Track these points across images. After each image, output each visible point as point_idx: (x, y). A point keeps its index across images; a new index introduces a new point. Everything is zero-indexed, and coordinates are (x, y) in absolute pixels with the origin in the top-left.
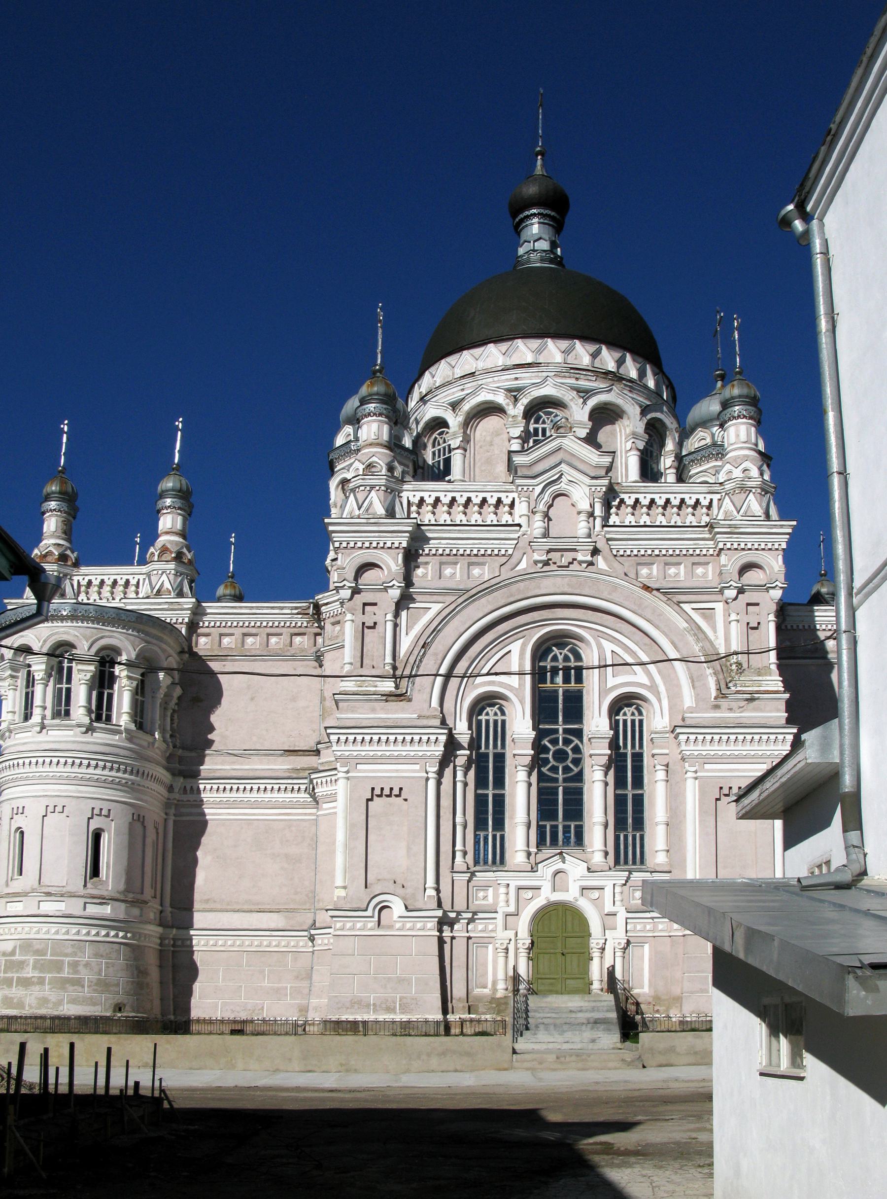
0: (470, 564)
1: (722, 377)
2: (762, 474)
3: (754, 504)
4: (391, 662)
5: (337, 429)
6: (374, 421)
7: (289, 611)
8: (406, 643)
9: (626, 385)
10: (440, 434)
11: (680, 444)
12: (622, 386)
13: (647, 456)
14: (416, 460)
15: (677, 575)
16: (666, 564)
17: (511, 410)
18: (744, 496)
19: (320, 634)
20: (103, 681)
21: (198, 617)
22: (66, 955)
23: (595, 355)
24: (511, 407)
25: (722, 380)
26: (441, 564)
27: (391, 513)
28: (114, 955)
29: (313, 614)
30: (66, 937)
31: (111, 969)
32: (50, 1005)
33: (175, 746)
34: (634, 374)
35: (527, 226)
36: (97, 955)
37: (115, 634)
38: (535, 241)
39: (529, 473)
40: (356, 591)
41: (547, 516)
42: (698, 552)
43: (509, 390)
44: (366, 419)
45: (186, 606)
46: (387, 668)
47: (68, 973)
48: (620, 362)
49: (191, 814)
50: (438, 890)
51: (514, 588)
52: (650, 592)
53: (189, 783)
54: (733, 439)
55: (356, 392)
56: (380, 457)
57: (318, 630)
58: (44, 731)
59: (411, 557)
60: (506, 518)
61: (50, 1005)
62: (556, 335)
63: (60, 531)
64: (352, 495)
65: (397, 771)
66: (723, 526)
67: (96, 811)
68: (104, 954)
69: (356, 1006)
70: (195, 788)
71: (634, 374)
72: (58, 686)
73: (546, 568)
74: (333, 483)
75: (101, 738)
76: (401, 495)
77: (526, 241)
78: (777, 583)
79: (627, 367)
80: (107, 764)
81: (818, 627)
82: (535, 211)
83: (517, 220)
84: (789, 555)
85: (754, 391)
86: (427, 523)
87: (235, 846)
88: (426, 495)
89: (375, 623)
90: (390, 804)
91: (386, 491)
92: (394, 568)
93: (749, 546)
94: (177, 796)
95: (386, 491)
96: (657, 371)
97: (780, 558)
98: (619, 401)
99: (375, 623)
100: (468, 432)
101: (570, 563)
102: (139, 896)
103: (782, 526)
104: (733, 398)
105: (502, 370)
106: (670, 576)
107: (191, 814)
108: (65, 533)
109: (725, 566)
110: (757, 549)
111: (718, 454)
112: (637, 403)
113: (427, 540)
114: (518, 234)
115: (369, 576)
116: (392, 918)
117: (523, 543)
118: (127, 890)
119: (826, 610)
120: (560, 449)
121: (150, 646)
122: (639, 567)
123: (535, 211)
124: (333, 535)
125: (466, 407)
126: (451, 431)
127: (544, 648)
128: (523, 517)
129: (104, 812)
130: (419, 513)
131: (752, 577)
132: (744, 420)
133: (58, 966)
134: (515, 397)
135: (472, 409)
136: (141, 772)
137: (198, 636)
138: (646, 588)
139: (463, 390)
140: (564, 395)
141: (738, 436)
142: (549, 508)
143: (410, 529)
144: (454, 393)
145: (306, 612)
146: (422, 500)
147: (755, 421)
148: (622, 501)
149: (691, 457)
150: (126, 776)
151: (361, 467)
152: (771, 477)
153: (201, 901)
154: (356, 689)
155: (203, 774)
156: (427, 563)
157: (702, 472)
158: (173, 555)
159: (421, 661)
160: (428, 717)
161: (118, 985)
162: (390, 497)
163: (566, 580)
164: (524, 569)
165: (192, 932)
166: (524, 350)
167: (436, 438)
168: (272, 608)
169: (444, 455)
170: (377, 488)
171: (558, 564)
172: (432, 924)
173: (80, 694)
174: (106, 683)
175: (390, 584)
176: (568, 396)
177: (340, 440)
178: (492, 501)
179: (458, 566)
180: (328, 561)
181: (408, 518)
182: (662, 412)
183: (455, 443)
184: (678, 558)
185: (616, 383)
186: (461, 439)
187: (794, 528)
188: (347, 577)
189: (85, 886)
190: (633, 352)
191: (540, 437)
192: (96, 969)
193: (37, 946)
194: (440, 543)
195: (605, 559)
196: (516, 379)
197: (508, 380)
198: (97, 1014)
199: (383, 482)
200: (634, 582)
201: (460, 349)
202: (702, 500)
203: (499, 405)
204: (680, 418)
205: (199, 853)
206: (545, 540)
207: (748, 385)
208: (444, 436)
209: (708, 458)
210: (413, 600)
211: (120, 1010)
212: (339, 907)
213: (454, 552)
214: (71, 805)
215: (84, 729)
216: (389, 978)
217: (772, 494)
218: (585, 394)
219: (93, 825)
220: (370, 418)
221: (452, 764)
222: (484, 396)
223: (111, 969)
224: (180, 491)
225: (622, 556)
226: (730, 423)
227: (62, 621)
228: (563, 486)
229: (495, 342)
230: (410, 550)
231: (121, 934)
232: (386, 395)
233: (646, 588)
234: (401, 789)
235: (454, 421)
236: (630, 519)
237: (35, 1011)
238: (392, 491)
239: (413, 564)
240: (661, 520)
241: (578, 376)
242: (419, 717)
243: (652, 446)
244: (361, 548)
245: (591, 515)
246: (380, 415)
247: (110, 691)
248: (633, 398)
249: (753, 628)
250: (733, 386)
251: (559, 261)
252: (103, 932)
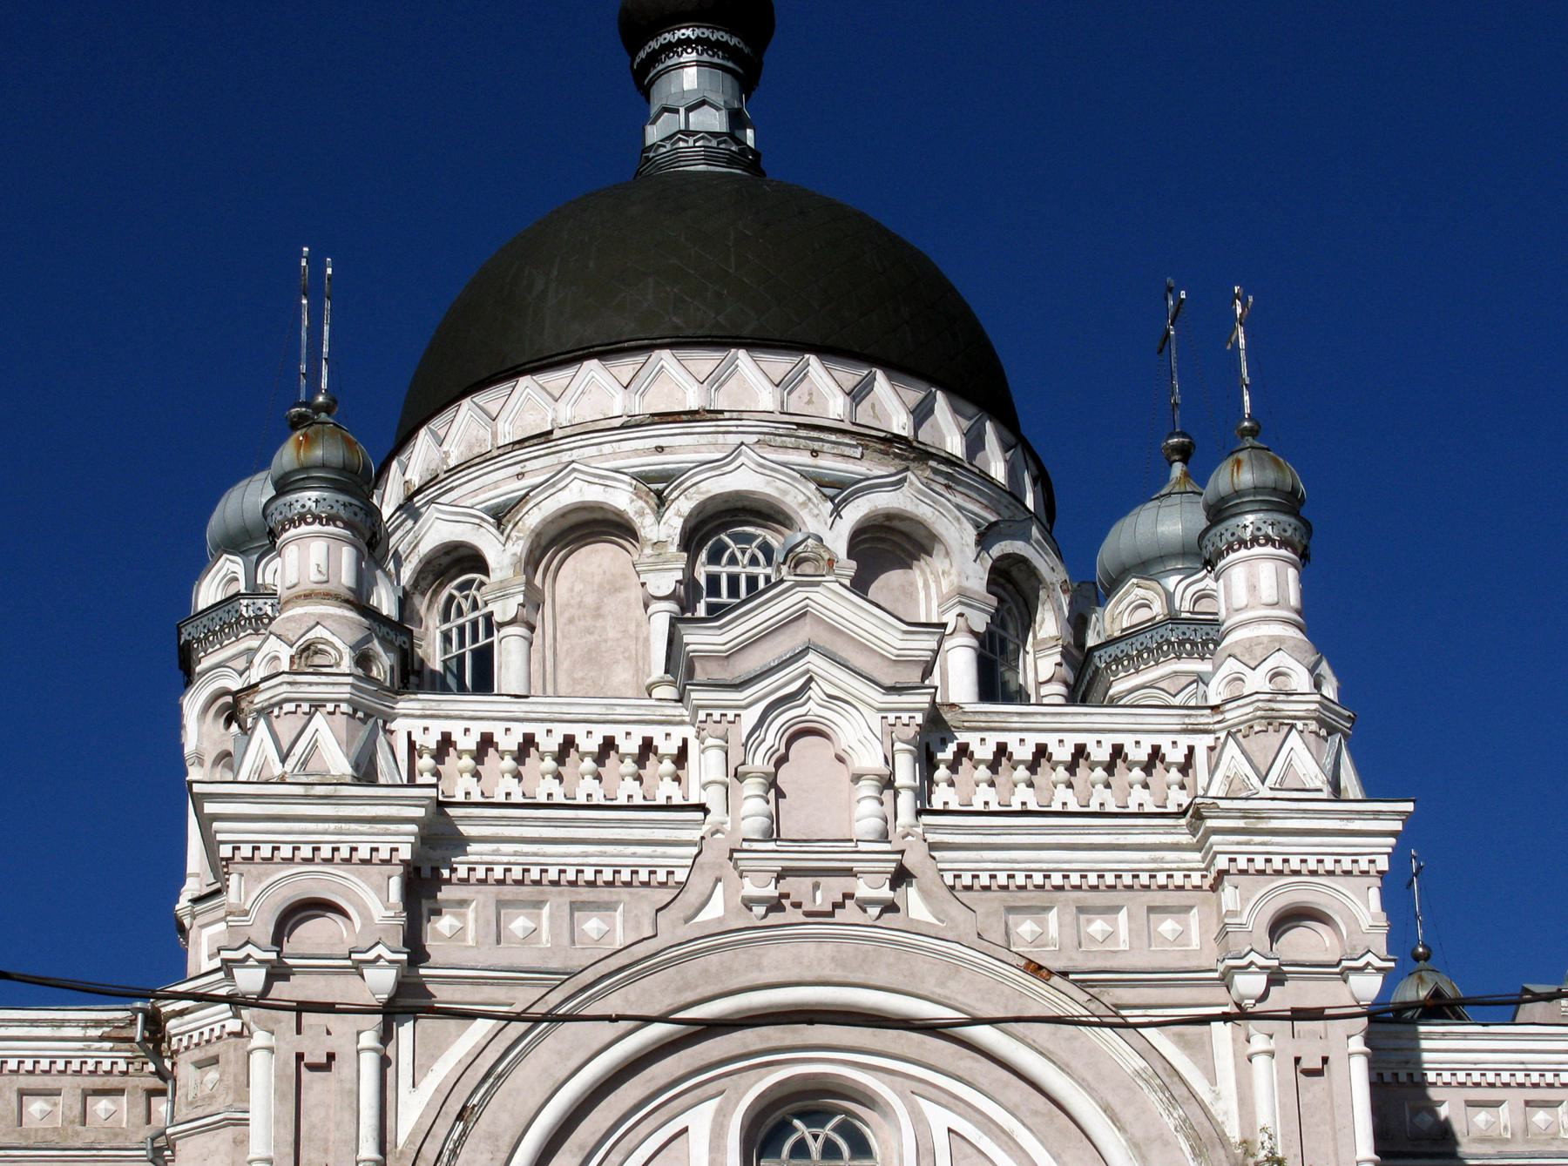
0: (575, 906)
1: (1185, 453)
2: (1317, 686)
3: (1303, 760)
4: (376, 1156)
5: (198, 566)
6: (317, 536)
7: (78, 1032)
8: (411, 1110)
9: (936, 471)
10: (463, 587)
11: (1078, 622)
12: (928, 473)
13: (992, 650)
14: (409, 651)
15: (1111, 936)
16: (1081, 910)
17: (648, 527)
18: (1274, 739)
19: (163, 1093)
23: (857, 395)
24: (650, 519)
25: (1185, 461)
26: (501, 904)
27: (365, 772)
29: (144, 1039)
34: (955, 445)
35: (667, 70)
38: (689, 110)
39: (726, 676)
40: (278, 972)
41: (772, 783)
42: (1161, 879)
43: (644, 478)
44: (293, 532)
48: (921, 413)
51: (693, 968)
52: (1046, 980)
54: (1240, 596)
55: (264, 464)
56: (337, 631)
57: (156, 1082)
59: (421, 887)
60: (666, 791)
62: (758, 343)
64: (262, 724)
66: (1228, 814)
71: (955, 445)
73: (774, 918)
74: (192, 704)
76: (392, 726)
77: (666, 109)
78: (1370, 958)
79: (936, 428)
81: (1431, 1077)
82: (689, 32)
83: (642, 55)
84: (1394, 888)
85: (1289, 477)
86: (460, 798)
88: (456, 729)
91: (352, 716)
92: (378, 912)
93: (1295, 864)
95: (352, 716)
96: (1011, 439)
97: (1374, 895)
98: (924, 511)
100: (538, 580)
101: (836, 906)
103: (1377, 815)
104: (1238, 493)
105: (622, 427)
106: (1092, 939)
109: (1234, 914)
110: (1313, 873)
111: (1181, 643)
112: (969, 519)
114: (646, 92)
115: (312, 934)
117: (715, 852)
119: (1465, 1036)
120: (803, 615)
122: (1012, 918)
123: (689, 32)
124: (216, 825)
125: (533, 518)
126: (496, 576)
127: (771, 1122)
128: (711, 788)
130: (437, 774)
131: (1303, 942)
132: (1269, 549)
134: (659, 494)
135: (548, 523)
138: (1036, 969)
139: (520, 476)
140: (785, 493)
141: (1253, 588)
142: (778, 764)
143: (421, 812)
144: (499, 485)
145: (125, 1033)
146: (446, 742)
147: (1295, 552)
148: (963, 750)
149: (1113, 650)
151: (285, 653)
152: (1340, 692)
156: (463, 903)
157: (1143, 687)
159: (454, 1154)
162: (363, 732)
163: (828, 948)
164: (720, 920)
166: (677, 377)
167: (451, 598)
168: (33, 1023)
169: (475, 639)
170: (330, 707)
171: (806, 907)
173: (908, 546)
175: (371, 955)
176: (795, 496)
177: (208, 593)
178: (630, 746)
179: (546, 911)
180: (183, 903)
181: (412, 783)
182: (1027, 538)
183: (504, 610)
184: (1112, 894)
185: (912, 465)
186: (520, 598)
187: (1408, 818)
188: (254, 934)
190: (948, 389)
191: (725, 598)
194: (496, 853)
195: (926, 895)
196: (660, 449)
197: (637, 452)
199: (345, 692)
200: (1004, 954)
201: (512, 373)
202: (1166, 749)
203: (619, 513)
204: (1078, 553)
206: (771, 846)
207: (1277, 463)
208: (473, 592)
209: (1157, 653)
213: (535, 874)
217: (1345, 735)
218: (837, 490)
220: (304, 529)
222: (576, 492)
225: (968, 888)
226: (1232, 556)
228: (812, 708)
229: (602, 355)
230: (418, 870)
232: (344, 469)
233: (1036, 969)
235: (502, 554)
236: (985, 796)
238: (368, 718)
239: (426, 905)
240: (1064, 798)
241: (816, 446)
243: (1004, 626)
244: (289, 861)
245: (888, 783)
246: (331, 520)
248: (958, 507)
249: (1309, 1073)
250: (1239, 463)
251: (751, 161)
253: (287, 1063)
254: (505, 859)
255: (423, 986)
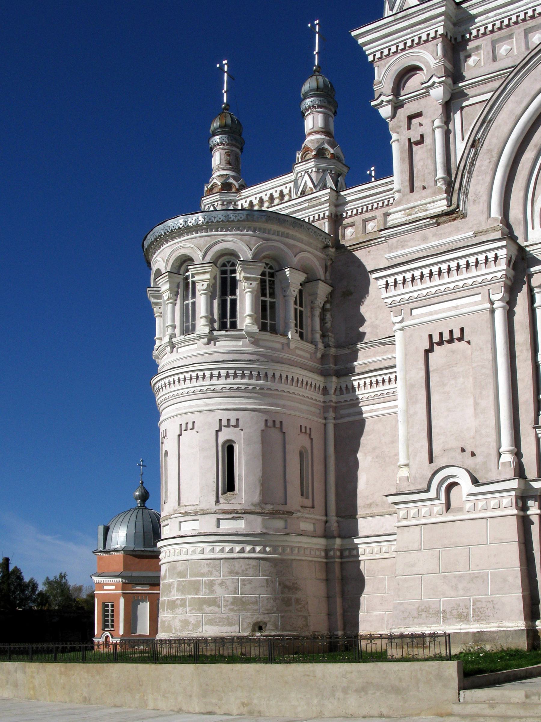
20: (226, 286)
21: (340, 209)
22: (203, 575)
28: (251, 572)
30: (212, 556)
31: (248, 587)
32: (191, 627)
33: (327, 346)
36: (232, 573)
37: (228, 238)
45: (323, 199)
46: (439, 185)
47: (205, 593)
49: (349, 415)
50: (518, 454)
53: (343, 382)
58: (175, 349)
61: (191, 627)
63: (224, 162)
65: (456, 307)
67: (224, 423)
68: (240, 571)
69: (424, 614)
70: (350, 387)
72: (185, 303)
75: (224, 346)
80: (230, 372)
87: (393, 442)
89: (422, 136)
90: (453, 352)
94: (334, 398)
99: (422, 136)
102: (281, 508)
107: (349, 415)
108: (229, 163)
113: (472, 19)
115: (414, 83)
116: (461, 497)
118: (264, 501)
121: (270, 243)
129: (233, 422)
133: (195, 587)
136: (284, 377)
137: (345, 228)
150: (253, 381)
153: (364, 507)
154: (405, 219)
155: (357, 371)
156: (478, 48)
158: (313, 153)
159: (472, 164)
160: (486, 232)
161: (257, 602)
165: (356, 541)
172: (508, 499)
174: (229, 290)
175: (430, 83)
188: (384, 91)
189: (217, 501)
192: (231, 588)
193: (180, 567)
198: (234, 634)
205: (360, 455)
210: (465, 96)
211: (260, 629)
212: (402, 490)
214: (199, 419)
215: (205, 340)
216: (461, 576)
219: (223, 437)
221: (525, 287)
223: (248, 587)
224: (318, 89)
227: (180, 236)
231: (258, 549)
234: (462, 330)
237: (179, 634)
239: (462, 55)
242: (476, 235)
244: (396, 53)
247: (233, 297)
252: (238, 548)
253: (404, 145)
254: (492, 20)
255: (462, 91)
